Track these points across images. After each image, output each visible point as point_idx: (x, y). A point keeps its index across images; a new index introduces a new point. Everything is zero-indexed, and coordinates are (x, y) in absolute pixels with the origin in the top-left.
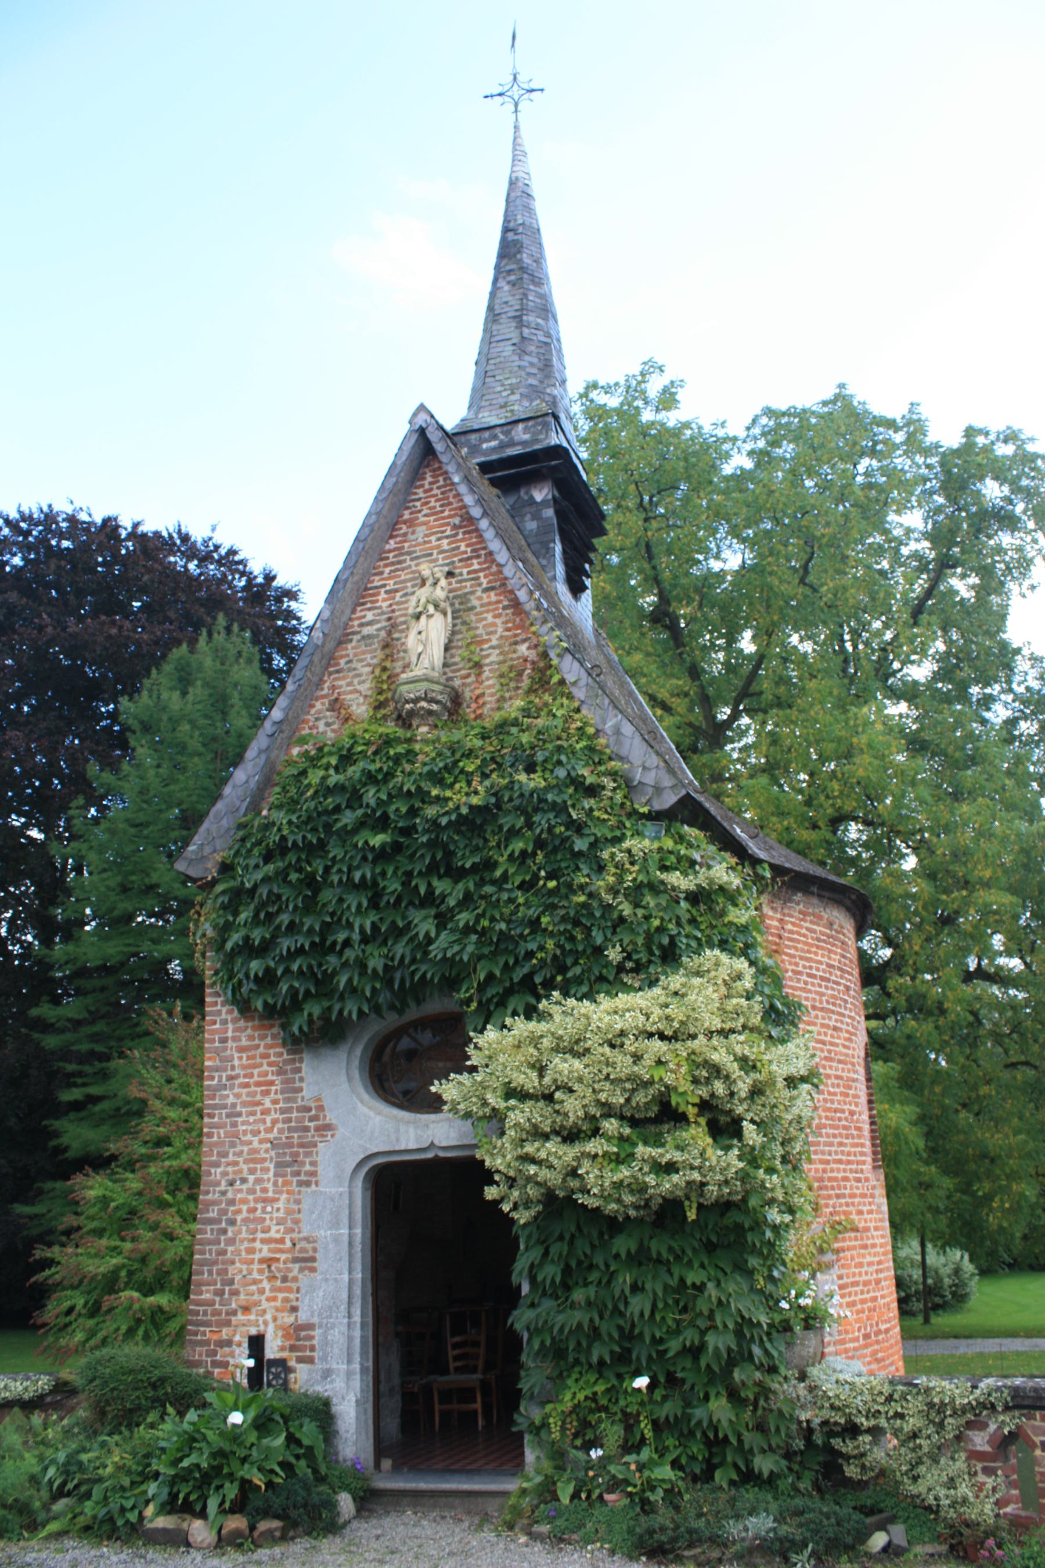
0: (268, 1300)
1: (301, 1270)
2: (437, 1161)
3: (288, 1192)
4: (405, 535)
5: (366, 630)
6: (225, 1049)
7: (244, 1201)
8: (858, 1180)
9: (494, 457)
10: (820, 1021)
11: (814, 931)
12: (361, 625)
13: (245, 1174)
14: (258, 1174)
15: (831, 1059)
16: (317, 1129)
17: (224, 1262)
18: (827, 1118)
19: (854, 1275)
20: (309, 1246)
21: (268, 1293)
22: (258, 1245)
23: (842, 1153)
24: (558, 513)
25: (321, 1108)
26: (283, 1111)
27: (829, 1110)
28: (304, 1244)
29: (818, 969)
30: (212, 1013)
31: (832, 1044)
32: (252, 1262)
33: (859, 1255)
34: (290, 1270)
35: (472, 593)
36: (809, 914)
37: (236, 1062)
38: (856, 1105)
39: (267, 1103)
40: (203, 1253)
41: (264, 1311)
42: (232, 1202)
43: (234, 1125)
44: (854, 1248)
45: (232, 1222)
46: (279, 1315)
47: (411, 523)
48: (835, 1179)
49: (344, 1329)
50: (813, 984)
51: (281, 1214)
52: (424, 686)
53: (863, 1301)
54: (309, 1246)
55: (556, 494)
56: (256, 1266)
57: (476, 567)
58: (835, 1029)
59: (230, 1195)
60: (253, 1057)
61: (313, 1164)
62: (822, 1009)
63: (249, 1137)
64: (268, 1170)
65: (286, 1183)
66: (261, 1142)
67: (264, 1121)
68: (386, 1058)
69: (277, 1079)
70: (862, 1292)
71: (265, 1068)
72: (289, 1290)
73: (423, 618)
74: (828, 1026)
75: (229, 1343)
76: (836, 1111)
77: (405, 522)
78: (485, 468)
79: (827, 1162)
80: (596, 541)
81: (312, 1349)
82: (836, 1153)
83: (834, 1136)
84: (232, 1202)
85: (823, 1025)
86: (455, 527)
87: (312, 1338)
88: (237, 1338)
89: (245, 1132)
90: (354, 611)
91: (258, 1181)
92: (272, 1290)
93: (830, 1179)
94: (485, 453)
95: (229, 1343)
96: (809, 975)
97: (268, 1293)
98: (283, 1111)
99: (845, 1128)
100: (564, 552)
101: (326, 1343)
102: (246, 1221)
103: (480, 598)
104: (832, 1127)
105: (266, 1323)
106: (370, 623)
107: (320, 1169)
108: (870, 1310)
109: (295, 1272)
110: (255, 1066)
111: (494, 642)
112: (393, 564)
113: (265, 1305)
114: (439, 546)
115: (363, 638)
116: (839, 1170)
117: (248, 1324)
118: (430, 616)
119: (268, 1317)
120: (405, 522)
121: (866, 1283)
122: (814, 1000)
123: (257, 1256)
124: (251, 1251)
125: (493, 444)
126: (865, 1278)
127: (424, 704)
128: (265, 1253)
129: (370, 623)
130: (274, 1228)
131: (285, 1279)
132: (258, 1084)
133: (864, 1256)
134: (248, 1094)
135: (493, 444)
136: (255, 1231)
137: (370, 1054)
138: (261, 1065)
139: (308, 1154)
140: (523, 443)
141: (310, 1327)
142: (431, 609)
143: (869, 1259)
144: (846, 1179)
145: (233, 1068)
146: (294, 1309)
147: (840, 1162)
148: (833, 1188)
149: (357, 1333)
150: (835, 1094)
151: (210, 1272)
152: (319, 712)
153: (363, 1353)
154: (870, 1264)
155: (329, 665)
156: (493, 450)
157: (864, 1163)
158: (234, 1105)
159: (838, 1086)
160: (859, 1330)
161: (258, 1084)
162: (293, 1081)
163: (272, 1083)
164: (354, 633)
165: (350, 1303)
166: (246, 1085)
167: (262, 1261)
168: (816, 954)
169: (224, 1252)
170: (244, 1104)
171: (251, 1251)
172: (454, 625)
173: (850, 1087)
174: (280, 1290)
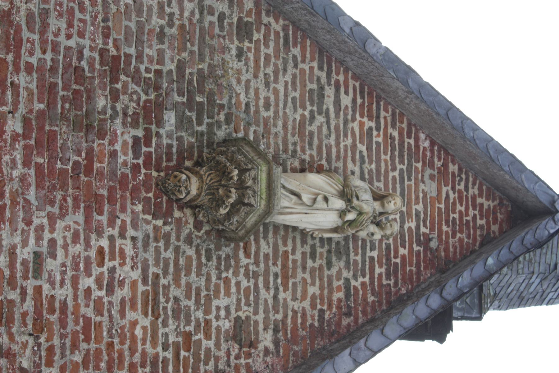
4: (432, 165)
47: (442, 175)
90: (356, 77)
106: (337, 102)
115: (322, 88)
120: (445, 166)
129: (337, 102)
142: (351, 216)
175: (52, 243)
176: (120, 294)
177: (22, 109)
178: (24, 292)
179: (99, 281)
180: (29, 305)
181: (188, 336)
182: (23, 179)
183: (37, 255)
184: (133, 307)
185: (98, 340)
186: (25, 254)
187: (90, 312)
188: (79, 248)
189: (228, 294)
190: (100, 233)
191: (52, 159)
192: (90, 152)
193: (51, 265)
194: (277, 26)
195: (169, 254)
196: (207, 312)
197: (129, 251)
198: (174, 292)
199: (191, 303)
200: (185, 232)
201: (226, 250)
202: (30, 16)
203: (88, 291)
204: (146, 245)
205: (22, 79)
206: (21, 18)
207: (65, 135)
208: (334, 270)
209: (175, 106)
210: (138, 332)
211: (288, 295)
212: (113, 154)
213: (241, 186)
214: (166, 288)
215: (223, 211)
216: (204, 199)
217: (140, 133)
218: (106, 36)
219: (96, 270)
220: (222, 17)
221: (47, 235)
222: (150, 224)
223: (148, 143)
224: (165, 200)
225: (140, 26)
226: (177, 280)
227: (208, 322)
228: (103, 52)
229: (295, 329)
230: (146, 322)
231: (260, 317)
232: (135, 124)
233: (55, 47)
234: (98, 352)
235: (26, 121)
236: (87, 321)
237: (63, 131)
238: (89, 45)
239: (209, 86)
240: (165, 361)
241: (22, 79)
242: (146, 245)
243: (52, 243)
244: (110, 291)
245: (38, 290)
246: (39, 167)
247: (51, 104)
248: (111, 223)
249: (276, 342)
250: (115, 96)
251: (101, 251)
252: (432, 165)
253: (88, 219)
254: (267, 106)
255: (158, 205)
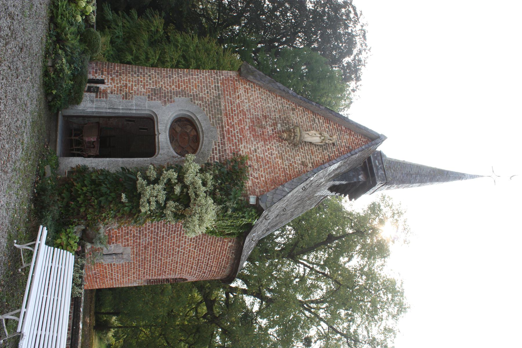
0: (115, 86)
1: (123, 95)
2: (154, 135)
3: (146, 92)
4: (346, 132)
5: (317, 120)
6: (190, 75)
7: (144, 79)
8: (144, 274)
9: (373, 164)
10: (194, 262)
11: (223, 262)
12: (318, 118)
13: (152, 80)
14: (152, 84)
15: (182, 265)
16: (165, 101)
17: (126, 73)
18: (164, 263)
19: (115, 270)
20: (130, 98)
21: (117, 85)
22: (131, 83)
23: (153, 268)
24: (355, 182)
25: (171, 102)
26: (171, 91)
27: (166, 264)
28: (131, 96)
29: (211, 262)
30: (200, 72)
31: (187, 265)
32: (126, 81)
33: (121, 272)
34: (123, 92)
35: (328, 151)
36: (228, 260)
37: (185, 78)
38: (168, 274)
39: (173, 87)
40: (129, 67)
41: (111, 84)
42: (144, 76)
43: (167, 77)
44: (123, 271)
45: (138, 76)
46: (110, 89)
47: (350, 134)
48: (145, 265)
49: (105, 107)
50: (206, 260)
51: (140, 90)
52: (299, 134)
53: (106, 272)
54: (130, 98)
55: (361, 183)
56: (125, 82)
57: (336, 153)
58: (192, 267)
59: (146, 75)
60: (187, 83)
61: (155, 100)
62: (198, 263)
63: (163, 81)
64: (153, 86)
65: (149, 91)
66: (162, 85)
67: (168, 86)
68: (185, 122)
69: (180, 90)
70: (109, 273)
71: (184, 86)
72: (117, 92)
73: (319, 135)
74: (193, 265)
75: (102, 74)
76: (166, 266)
77: (350, 132)
78: (369, 159)
79: (150, 262)
80: (347, 197)
81: (100, 98)
82: (153, 265)
83: (158, 265)
84: (144, 76)
85: (193, 263)
86: (349, 147)
87: (103, 98)
88: (104, 76)
89: (164, 80)
90: (322, 116)
91: (150, 83)
92: (118, 87)
93: (145, 262)
94: (374, 161)
95: (102, 74)
96: (209, 259)
97: (117, 85)
98: (171, 91)
99: (161, 269)
100: (343, 185)
101: (102, 101)
102: (138, 80)
103: (326, 153)
104: (161, 264)
105: (108, 85)
106: (319, 121)
107: (153, 101)
108: (104, 275)
109: (123, 93)
110: (184, 83)
111: (312, 157)
112: (337, 128)
113: (113, 84)
114: (342, 141)
115: (314, 119)
116: (147, 266)
117: (108, 80)
118: (320, 137)
119: (110, 85)
120: (350, 132)
121: (112, 274)
122: (201, 260)
123: (128, 83)
124: (129, 81)
125: (377, 164)
126: (113, 274)
127: (293, 135)
128: (129, 85)
129: (319, 121)
130: (136, 88)
131: (121, 90)
132: (179, 84)
133: (120, 274)
134: (176, 81)
135: (377, 164)
136: (135, 82)
137: (189, 118)
138: (184, 85)
139: (158, 98)
140: (378, 173)
141: (106, 98)
142: (323, 138)
143: (119, 276)
144: (145, 269)
145: (184, 77)
146: (112, 93)
147: (150, 267)
148: (142, 263)
149: (103, 110)
150: (171, 266)
151: (123, 69)
152: (292, 105)
153: (98, 112)
154: (118, 276)
155: (306, 109)
156: (375, 164)
157: (149, 276)
158: (173, 77)
159: (174, 267)
160: (98, 271)
161: (179, 84)
162: (180, 94)
163: (179, 88)
164: (316, 116)
165: (113, 109)
166: (178, 81)
167: (126, 84)
168: (216, 262)
169: (129, 73)
170: (173, 80)
171: (129, 81)
172: (318, 145)
173: (173, 272)
174: (117, 89)
175: (258, 147)
176: (274, 156)
177: (248, 125)
178: (253, 155)
179: (269, 154)
180: (255, 157)
181: (291, 164)
182: (250, 136)
183: (255, 149)
184: (277, 158)
185: (271, 164)
186: (253, 149)
187: (268, 159)
188: (263, 148)
189: (299, 156)
190: (267, 145)
191: (255, 133)
192: (263, 132)
193: (258, 151)
194: (302, 108)
195: (284, 149)
196: (294, 159)
197: (274, 148)
198: (286, 156)
199: (290, 158)
200: (286, 145)
201: (296, 149)
202: (247, 110)
203: (267, 156)
204: (278, 147)
205: (247, 120)
206: (245, 110)
207: (257, 129)
208: (325, 153)
209: (280, 123)
210: (279, 163)
211: (314, 157)
212: (268, 132)
213: (294, 132)
214: (284, 155)
215: (292, 138)
216: (288, 137)
217: (273, 128)
218: (263, 112)
219: (268, 152)
220: (288, 108)
221: (256, 146)
222: (278, 144)
223: (275, 129)
224: (281, 139)
225: (270, 110)
226: (286, 154)
227: (295, 162)
228: (263, 115)
229: (317, 163)
230: (281, 161)
231: (308, 161)
232: (272, 126)
233: (253, 114)
234: (271, 166)
235: (249, 127)
236: (268, 161)
237: (257, 129)
238: (260, 114)
239: (287, 119)
240: (286, 168)
241: (247, 120)
242: (278, 147)
243: (258, 147)
244: (272, 155)
245: (256, 155)
246: (253, 135)
247: (254, 124)
248: (270, 143)
249: (313, 166)
250: (266, 122)
251: (268, 148)
252: (346, 132)
253: (265, 143)
254: (301, 122)
255: (279, 141)
